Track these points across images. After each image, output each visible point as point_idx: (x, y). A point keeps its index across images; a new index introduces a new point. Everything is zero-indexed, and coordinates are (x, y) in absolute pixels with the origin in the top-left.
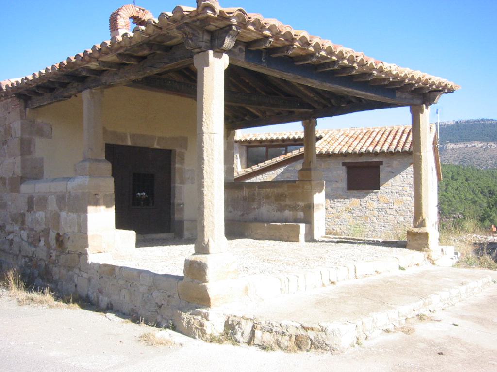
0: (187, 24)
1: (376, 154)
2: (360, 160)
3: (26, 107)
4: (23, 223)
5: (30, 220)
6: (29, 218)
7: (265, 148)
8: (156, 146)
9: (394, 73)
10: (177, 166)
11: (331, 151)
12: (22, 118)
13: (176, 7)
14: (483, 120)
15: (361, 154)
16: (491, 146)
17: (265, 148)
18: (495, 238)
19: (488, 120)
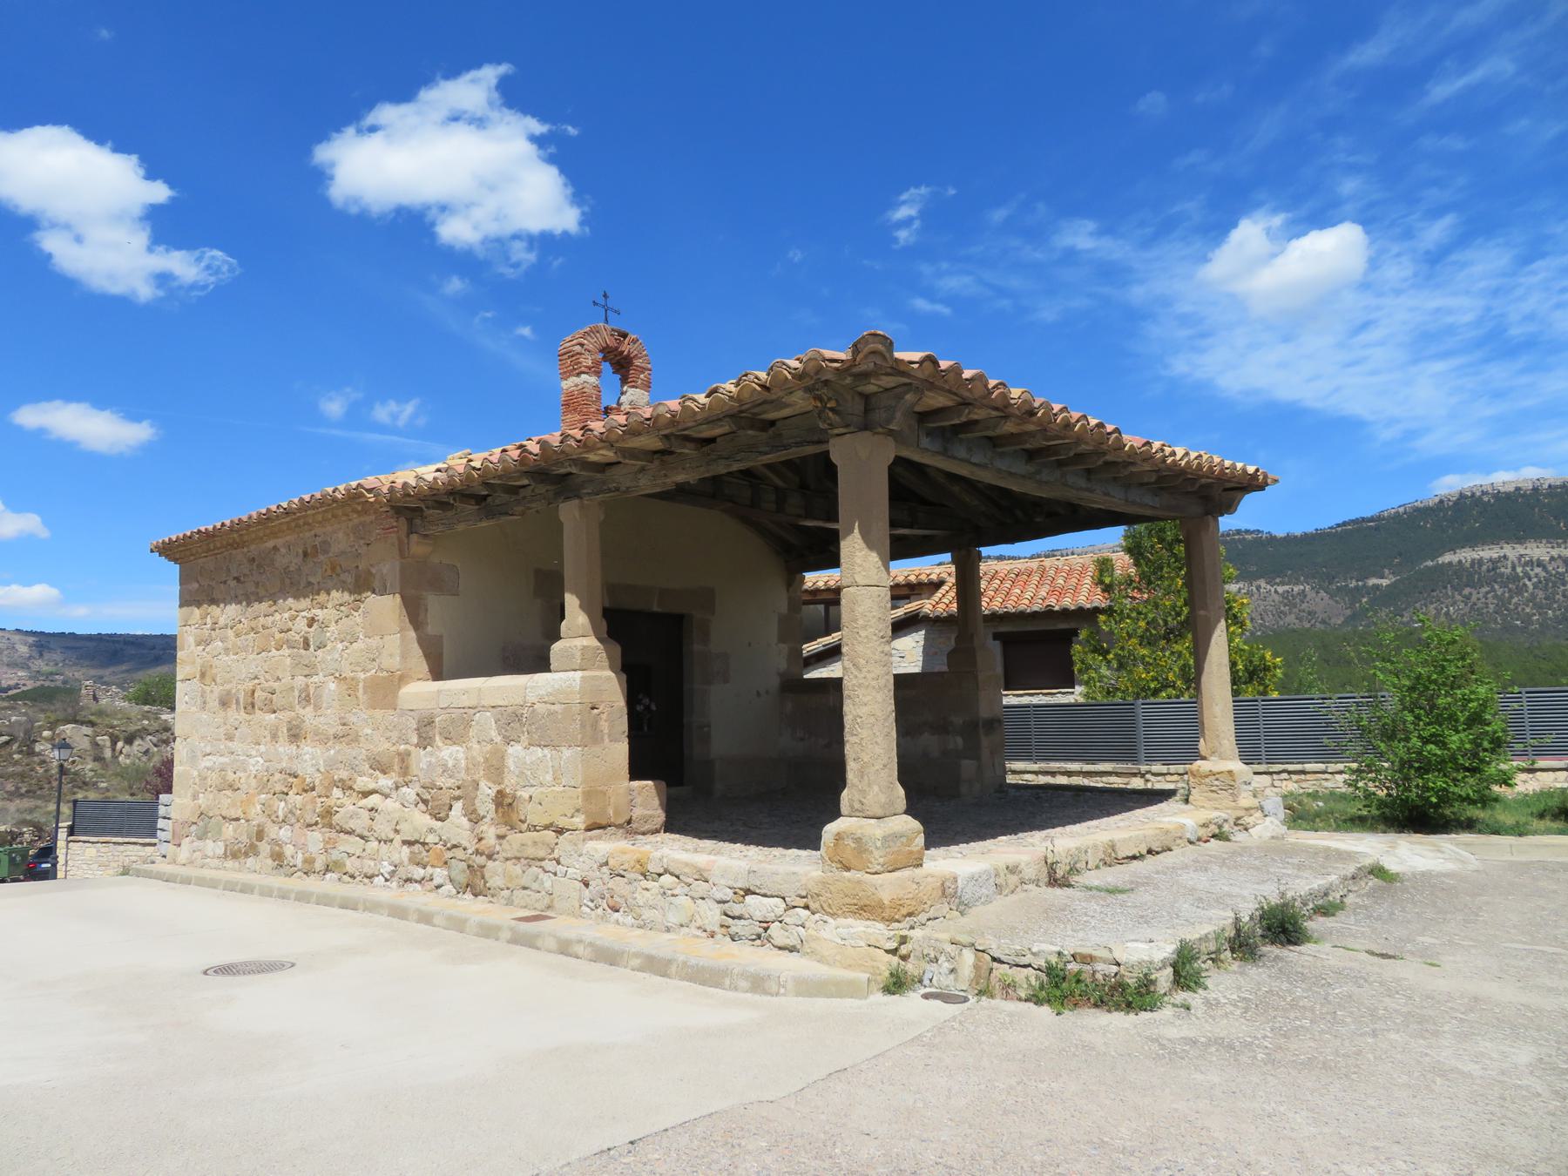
0: (826, 383)
1: (1065, 612)
2: (1030, 628)
3: (410, 532)
4: (405, 771)
5: (423, 765)
6: (421, 760)
7: (821, 607)
8: (656, 609)
9: (681, 958)
10: (697, 647)
11: (912, 578)
12: (402, 556)
13: (890, 468)
14: (1238, 532)
15: (1035, 615)
16: (1258, 588)
17: (821, 607)
18: (1566, 1085)
19: (1247, 532)
